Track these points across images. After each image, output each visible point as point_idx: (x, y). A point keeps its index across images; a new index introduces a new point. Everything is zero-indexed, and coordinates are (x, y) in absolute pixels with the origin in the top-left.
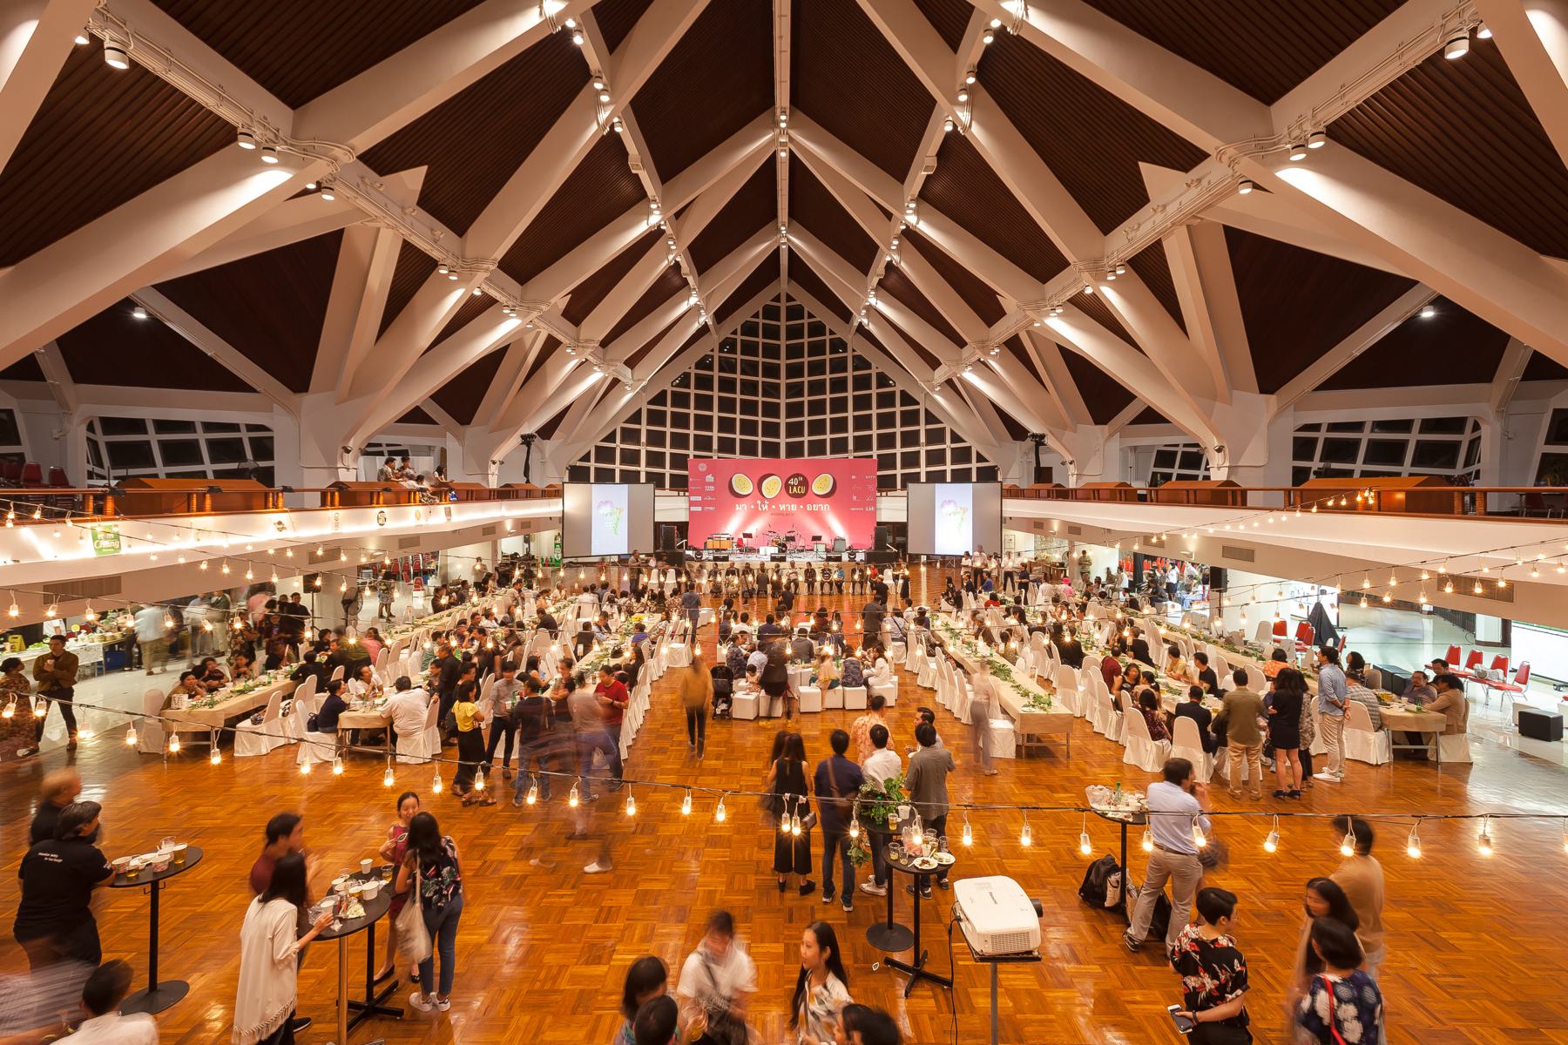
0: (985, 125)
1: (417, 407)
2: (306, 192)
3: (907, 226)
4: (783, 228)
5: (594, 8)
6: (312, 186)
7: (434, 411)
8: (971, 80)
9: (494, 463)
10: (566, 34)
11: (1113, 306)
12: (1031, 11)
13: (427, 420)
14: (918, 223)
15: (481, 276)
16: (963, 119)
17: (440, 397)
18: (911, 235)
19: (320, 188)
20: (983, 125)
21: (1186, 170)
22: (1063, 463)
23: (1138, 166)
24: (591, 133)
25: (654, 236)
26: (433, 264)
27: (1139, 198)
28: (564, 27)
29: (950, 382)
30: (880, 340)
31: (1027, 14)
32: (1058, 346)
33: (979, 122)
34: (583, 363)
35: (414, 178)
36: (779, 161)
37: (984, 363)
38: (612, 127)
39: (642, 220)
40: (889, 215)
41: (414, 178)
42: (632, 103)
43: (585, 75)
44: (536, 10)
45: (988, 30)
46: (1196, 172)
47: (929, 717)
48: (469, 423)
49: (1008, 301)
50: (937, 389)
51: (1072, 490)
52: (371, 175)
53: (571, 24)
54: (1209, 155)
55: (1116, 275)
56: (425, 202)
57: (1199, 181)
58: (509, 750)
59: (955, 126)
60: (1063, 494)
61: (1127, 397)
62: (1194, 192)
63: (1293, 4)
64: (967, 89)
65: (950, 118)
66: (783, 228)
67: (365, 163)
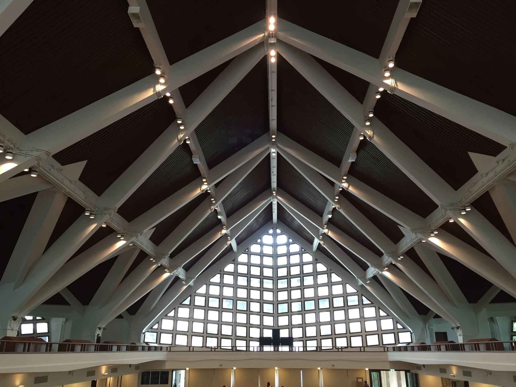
0: (380, 136)
1: (58, 293)
2: (24, 173)
3: (343, 188)
4: (274, 192)
5: (179, 88)
6: (27, 170)
7: (69, 297)
8: (371, 115)
9: (100, 329)
10: (166, 99)
11: (459, 259)
12: (399, 84)
13: (65, 303)
14: (349, 187)
15: (106, 218)
16: (369, 134)
17: (72, 288)
18: (344, 193)
19: (31, 171)
20: (379, 136)
21: (495, 155)
22: (453, 328)
23: (468, 154)
24: (175, 144)
25: (205, 195)
26: (83, 210)
27: (472, 171)
28: (165, 96)
29: (375, 278)
30: (402, 90)
31: (397, 85)
32: (437, 253)
33: (400, 81)
34: (159, 267)
35: (79, 167)
36: (271, 157)
37: (394, 265)
38: (185, 141)
39: (198, 188)
40: (332, 184)
41: (79, 167)
42: (196, 130)
43: (174, 118)
44: (152, 89)
45: (261, 350)
46: (501, 155)
47: (424, 367)
48: (88, 304)
49: (405, 229)
50: (368, 282)
51: (461, 344)
52: (57, 165)
53: (168, 94)
54: (506, 147)
55: (466, 211)
56: (82, 179)
57: (503, 160)
58: (263, 215)
59: (365, 137)
60: (456, 348)
61: (487, 285)
62: (501, 166)
63: (515, 160)
64: (370, 120)
65: (362, 134)
66: (274, 192)
67: (55, 159)
